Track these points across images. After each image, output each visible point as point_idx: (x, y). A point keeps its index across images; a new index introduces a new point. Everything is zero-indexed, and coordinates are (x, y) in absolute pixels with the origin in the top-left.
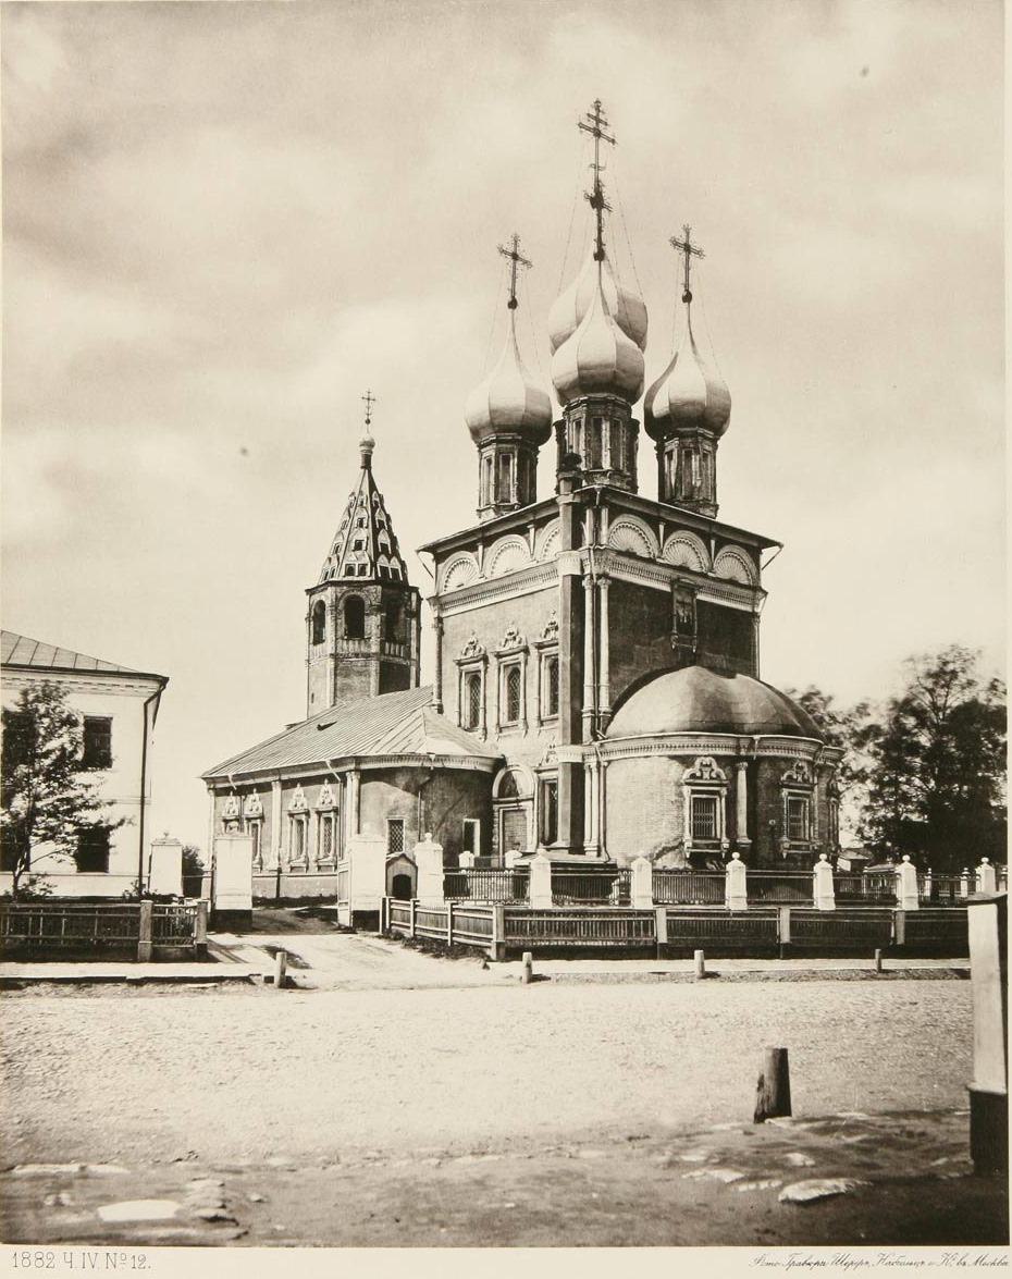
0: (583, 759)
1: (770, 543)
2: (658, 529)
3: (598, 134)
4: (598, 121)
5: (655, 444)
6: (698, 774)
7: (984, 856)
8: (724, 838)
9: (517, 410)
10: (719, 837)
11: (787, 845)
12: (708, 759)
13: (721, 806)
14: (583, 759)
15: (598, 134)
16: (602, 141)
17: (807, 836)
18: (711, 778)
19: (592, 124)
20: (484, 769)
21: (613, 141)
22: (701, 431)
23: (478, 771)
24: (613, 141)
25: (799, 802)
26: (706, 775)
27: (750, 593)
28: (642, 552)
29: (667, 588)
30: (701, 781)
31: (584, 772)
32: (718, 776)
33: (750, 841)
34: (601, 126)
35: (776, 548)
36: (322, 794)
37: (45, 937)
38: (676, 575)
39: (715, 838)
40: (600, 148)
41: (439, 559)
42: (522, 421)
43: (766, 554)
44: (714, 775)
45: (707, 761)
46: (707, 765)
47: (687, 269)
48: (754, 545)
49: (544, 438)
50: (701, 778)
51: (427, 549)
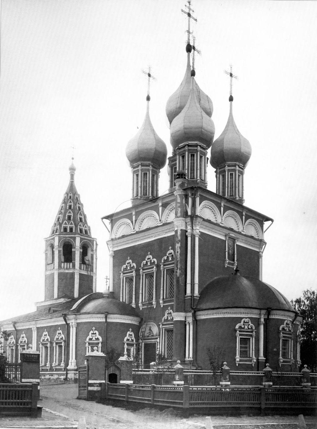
0: (186, 319)
1: (268, 219)
2: (221, 208)
3: (189, 15)
4: (190, 9)
5: (215, 170)
6: (243, 327)
7: (37, 388)
8: (254, 357)
9: (151, 149)
10: (251, 356)
11: (282, 361)
12: (247, 319)
13: (253, 341)
14: (186, 319)
15: (189, 15)
16: (191, 19)
17: (290, 358)
18: (249, 328)
19: (187, 11)
20: (137, 324)
21: (196, 20)
22: (237, 163)
23: (132, 324)
24: (196, 20)
25: (287, 340)
26: (246, 327)
27: (259, 242)
28: (213, 220)
29: (223, 238)
30: (244, 330)
31: (186, 325)
32: (252, 328)
33: (265, 359)
34: (191, 13)
35: (270, 222)
36: (57, 334)
37: (152, 396)
38: (227, 232)
39: (250, 357)
40: (191, 23)
41: (113, 223)
42: (155, 153)
43: (266, 224)
44: (250, 327)
45: (246, 320)
46: (247, 322)
47: (231, 85)
48: (261, 219)
49: (162, 164)
50: (244, 328)
51: (107, 218)
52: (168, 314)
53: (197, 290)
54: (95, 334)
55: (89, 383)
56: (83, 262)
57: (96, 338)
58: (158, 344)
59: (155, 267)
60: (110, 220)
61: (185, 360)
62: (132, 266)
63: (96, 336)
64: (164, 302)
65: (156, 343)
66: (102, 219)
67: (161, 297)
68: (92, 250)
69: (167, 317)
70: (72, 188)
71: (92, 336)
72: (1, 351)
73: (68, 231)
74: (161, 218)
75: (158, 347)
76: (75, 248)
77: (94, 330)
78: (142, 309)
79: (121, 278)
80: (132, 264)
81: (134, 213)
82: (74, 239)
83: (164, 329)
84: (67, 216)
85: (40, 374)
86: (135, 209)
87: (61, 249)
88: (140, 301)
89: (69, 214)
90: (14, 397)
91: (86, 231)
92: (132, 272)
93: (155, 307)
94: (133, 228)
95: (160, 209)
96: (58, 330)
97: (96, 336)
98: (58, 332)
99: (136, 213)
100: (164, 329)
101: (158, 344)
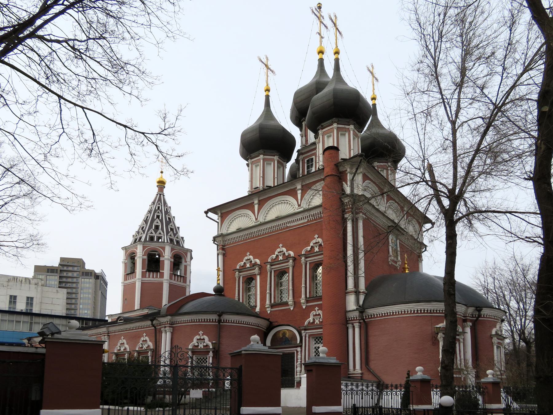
41: (223, 217)
51: (214, 210)
52: (314, 316)
53: (364, 284)
54: (204, 339)
55: (241, 413)
56: (173, 274)
57: (205, 344)
58: (299, 353)
59: (291, 261)
60: (219, 215)
61: (349, 373)
62: (253, 262)
63: (204, 342)
64: (307, 301)
65: (294, 353)
66: (206, 212)
67: (303, 296)
68: (186, 262)
69: (314, 319)
70: (160, 199)
71: (197, 342)
72: (166, 413)
73: (155, 240)
74: (301, 203)
75: (299, 357)
76: (164, 257)
77: (201, 334)
78: (271, 311)
79: (237, 277)
80: (252, 261)
81: (256, 202)
82: (164, 249)
83: (307, 336)
84: (154, 226)
85: (453, 377)
86: (259, 197)
87: (146, 257)
88: (268, 302)
89: (158, 214)
90: (392, 215)
91: (178, 242)
92: (254, 269)
93: (292, 309)
94: (254, 220)
95: (299, 192)
96: (143, 336)
97: (204, 342)
98: (142, 340)
99: (259, 201)
100: (307, 336)
101: (299, 353)
